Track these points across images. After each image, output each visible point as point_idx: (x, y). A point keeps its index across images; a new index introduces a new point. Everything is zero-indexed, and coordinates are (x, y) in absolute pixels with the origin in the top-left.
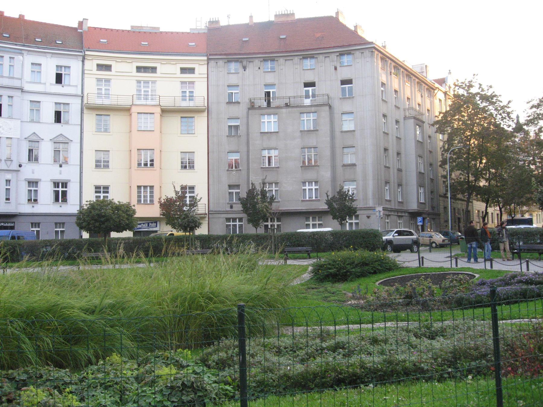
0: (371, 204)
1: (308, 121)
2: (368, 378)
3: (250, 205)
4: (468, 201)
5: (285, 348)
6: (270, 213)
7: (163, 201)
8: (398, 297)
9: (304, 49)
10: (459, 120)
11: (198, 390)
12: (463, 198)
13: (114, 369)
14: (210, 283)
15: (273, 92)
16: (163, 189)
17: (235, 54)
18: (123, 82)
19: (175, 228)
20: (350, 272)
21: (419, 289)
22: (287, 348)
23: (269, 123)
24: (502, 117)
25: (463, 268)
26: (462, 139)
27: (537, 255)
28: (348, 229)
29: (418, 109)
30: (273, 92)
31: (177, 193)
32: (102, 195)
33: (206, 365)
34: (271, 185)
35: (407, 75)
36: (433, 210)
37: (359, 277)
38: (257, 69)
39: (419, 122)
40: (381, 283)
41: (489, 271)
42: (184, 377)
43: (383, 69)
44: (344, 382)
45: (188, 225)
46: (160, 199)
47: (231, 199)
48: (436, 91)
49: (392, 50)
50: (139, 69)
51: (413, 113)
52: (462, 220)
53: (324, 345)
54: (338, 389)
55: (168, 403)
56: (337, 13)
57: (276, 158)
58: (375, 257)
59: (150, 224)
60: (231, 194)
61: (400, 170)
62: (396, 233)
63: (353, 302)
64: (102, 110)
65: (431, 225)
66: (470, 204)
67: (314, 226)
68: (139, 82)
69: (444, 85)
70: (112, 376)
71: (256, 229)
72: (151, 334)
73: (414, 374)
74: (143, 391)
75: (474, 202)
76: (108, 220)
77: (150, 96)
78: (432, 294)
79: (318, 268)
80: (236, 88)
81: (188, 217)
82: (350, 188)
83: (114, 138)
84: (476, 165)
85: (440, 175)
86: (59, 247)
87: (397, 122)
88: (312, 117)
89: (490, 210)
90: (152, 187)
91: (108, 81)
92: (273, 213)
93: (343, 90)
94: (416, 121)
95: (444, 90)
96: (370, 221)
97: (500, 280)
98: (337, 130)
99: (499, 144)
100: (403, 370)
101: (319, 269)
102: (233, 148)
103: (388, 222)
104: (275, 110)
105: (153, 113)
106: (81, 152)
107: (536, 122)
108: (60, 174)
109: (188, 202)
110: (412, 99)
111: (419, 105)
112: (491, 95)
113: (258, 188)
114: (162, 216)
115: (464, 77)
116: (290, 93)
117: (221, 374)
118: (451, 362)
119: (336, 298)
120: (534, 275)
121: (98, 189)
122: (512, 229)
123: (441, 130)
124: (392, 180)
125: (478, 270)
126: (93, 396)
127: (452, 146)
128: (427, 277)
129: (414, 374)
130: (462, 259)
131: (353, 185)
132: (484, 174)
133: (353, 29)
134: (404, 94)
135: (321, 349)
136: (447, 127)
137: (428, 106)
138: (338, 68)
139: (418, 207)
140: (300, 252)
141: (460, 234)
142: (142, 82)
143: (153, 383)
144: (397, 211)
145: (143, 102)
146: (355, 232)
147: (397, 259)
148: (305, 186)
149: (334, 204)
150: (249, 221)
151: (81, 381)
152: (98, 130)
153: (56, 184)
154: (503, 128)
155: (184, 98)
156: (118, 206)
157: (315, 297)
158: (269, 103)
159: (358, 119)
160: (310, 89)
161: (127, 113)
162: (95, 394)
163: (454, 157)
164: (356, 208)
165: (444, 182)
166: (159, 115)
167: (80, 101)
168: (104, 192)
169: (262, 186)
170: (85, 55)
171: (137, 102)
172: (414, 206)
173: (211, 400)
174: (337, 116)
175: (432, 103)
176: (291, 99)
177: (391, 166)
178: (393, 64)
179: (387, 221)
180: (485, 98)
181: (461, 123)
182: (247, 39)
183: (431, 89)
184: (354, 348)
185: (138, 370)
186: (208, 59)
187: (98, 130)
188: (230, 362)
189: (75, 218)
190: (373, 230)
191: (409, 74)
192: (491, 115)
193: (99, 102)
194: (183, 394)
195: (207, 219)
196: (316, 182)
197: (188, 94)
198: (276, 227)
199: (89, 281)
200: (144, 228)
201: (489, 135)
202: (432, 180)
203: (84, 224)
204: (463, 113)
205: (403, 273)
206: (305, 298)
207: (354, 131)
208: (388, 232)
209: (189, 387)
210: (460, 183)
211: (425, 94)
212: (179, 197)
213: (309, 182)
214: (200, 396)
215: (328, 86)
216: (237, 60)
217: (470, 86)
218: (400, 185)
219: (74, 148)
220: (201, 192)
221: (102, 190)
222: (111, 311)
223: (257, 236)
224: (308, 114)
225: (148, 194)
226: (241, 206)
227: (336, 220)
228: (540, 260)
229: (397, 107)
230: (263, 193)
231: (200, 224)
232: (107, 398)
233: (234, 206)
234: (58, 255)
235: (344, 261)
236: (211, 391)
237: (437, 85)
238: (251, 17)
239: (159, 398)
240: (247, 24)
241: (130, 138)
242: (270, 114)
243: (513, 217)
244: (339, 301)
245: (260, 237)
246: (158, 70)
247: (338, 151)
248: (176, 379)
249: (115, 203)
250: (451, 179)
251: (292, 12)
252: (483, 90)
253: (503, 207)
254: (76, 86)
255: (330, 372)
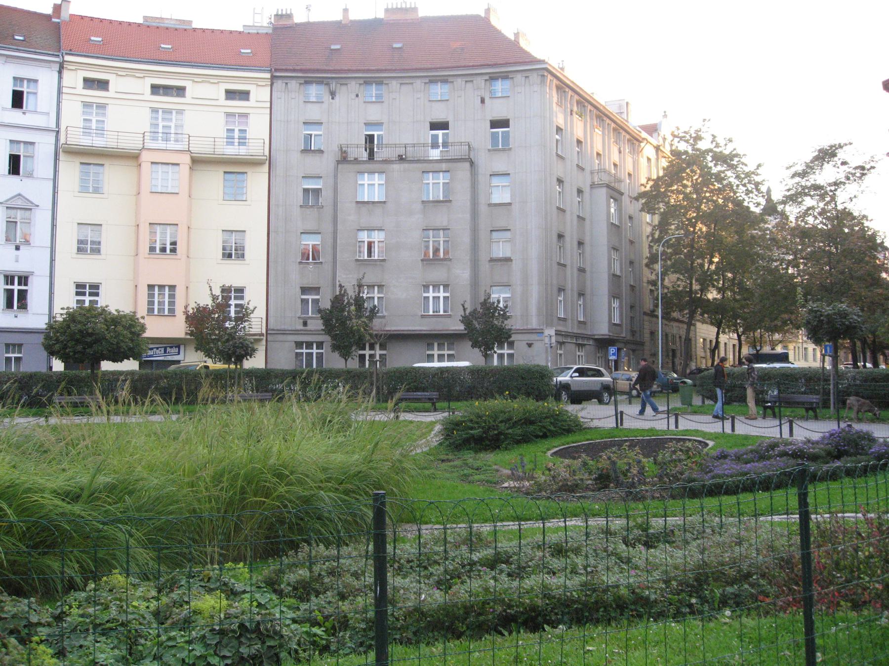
0: (534, 324)
1: (434, 185)
2: (556, 614)
3: (337, 320)
4: (690, 324)
5: (409, 561)
6: (371, 335)
7: (191, 311)
8: (586, 476)
9: (433, 66)
10: (678, 192)
11: (268, 636)
12: (681, 318)
13: (116, 599)
14: (276, 449)
15: (378, 136)
16: (190, 290)
17: (318, 71)
18: (128, 109)
19: (210, 357)
20: (506, 435)
21: (621, 464)
22: (412, 561)
23: (371, 186)
24: (747, 190)
25: (687, 430)
26: (682, 222)
27: (802, 412)
28: (496, 362)
29: (613, 172)
30: (378, 136)
31: (214, 298)
32: (87, 299)
33: (275, 591)
34: (371, 290)
35: (598, 117)
36: (633, 335)
37: (518, 442)
38: (354, 96)
39: (615, 193)
40: (555, 453)
41: (729, 436)
42: (243, 613)
43: (559, 104)
44: (516, 622)
45: (234, 353)
46: (186, 307)
47: (305, 310)
48: (642, 145)
49: (574, 75)
50: (156, 89)
51: (606, 179)
52: (678, 354)
53: (476, 557)
54: (506, 633)
55: (214, 660)
56: (488, 11)
57: (381, 245)
58: (546, 411)
59: (168, 349)
60: (304, 302)
61: (582, 270)
62: (575, 371)
63: (512, 484)
64: (91, 157)
65: (629, 360)
66: (692, 327)
67: (441, 358)
68: (155, 111)
69: (655, 135)
70: (113, 611)
71: (346, 360)
72: (178, 540)
73: (633, 607)
74: (170, 639)
75: (699, 325)
76: (98, 341)
77: (173, 135)
78: (642, 471)
79: (452, 426)
80: (317, 127)
81: (234, 338)
82: (499, 296)
83: (109, 204)
84: (702, 265)
85: (645, 280)
86: (16, 384)
87: (580, 192)
88: (442, 179)
89: (723, 338)
90: (172, 288)
91: (102, 107)
92: (376, 335)
93: (494, 137)
94: (611, 191)
95: (655, 143)
96: (533, 351)
97: (751, 451)
98: (482, 200)
99: (740, 232)
100: (614, 600)
101: (454, 429)
102: (311, 226)
103: (561, 355)
104: (381, 165)
105: (178, 164)
106: (54, 226)
107: (800, 200)
108: (17, 261)
109: (233, 314)
110: (604, 156)
111: (615, 165)
112: (731, 153)
113: (351, 293)
114: (188, 337)
115: (688, 123)
116: (407, 139)
117: (304, 606)
118: (692, 586)
119: (482, 477)
120: (805, 443)
121: (80, 288)
122: (762, 368)
123: (649, 208)
124: (569, 286)
125: (711, 434)
126: (81, 646)
127: (667, 233)
128: (633, 445)
129: (633, 607)
130: (686, 416)
131: (506, 293)
132: (716, 280)
133: (512, 38)
134: (592, 147)
135: (469, 564)
136: (659, 202)
137: (629, 168)
138: (487, 100)
139: (609, 331)
140: (418, 400)
141: (675, 376)
142: (160, 111)
143: (186, 624)
144: (577, 336)
145: (161, 145)
146: (508, 369)
147: (580, 415)
148: (428, 292)
149: (475, 322)
150: (335, 348)
151: (59, 618)
152: (84, 189)
153: (9, 279)
154: (748, 208)
155: (230, 141)
156: (117, 318)
157: (448, 475)
158: (371, 154)
159: (517, 185)
160: (440, 133)
161: (133, 163)
162: (86, 643)
163: (669, 251)
164: (510, 329)
165: (651, 291)
166: (188, 167)
167: (54, 138)
168: (91, 294)
169: (357, 288)
170: (64, 61)
171: (150, 144)
172: (602, 329)
173: (290, 653)
174: (482, 179)
175: (636, 164)
176: (408, 149)
177: (568, 263)
178: (576, 97)
179: (559, 352)
180: (720, 158)
181: (681, 197)
182: (338, 47)
183: (634, 141)
184: (526, 563)
185: (157, 599)
186: (273, 78)
187: (84, 189)
188: (317, 586)
189: (42, 336)
190: (538, 366)
191: (601, 115)
192: (730, 185)
193: (86, 141)
194: (241, 643)
195: (264, 342)
196: (446, 287)
197: (236, 134)
198: (378, 358)
199: (67, 444)
200: (158, 356)
201: (725, 217)
202: (632, 287)
203: (57, 347)
204: (685, 182)
205: (589, 437)
206: (433, 477)
207: (510, 204)
208: (563, 370)
209: (253, 632)
210: (676, 293)
211: (625, 149)
212: (219, 306)
213: (434, 286)
214: (270, 647)
215: (470, 130)
216: (320, 81)
217: (698, 138)
218: (581, 294)
219: (42, 219)
220: (255, 298)
221: (87, 290)
222: (108, 497)
223: (349, 372)
224: (436, 175)
225: (167, 300)
226: (321, 322)
227: (477, 350)
228: (807, 419)
229: (581, 168)
230: (359, 302)
231: (254, 350)
232: (107, 652)
233: (309, 322)
234: (13, 398)
235: (495, 416)
236: (290, 638)
237: (644, 135)
238: (346, 11)
239: (199, 650)
240: (340, 22)
241: (138, 204)
242: (373, 172)
243: (758, 351)
244: (487, 481)
245: (352, 374)
246: (188, 92)
247: (483, 234)
248: (228, 617)
249: (110, 313)
250: (663, 286)
251: (413, 6)
252: (717, 146)
253: (743, 333)
254: (48, 114)
255: (492, 604)
